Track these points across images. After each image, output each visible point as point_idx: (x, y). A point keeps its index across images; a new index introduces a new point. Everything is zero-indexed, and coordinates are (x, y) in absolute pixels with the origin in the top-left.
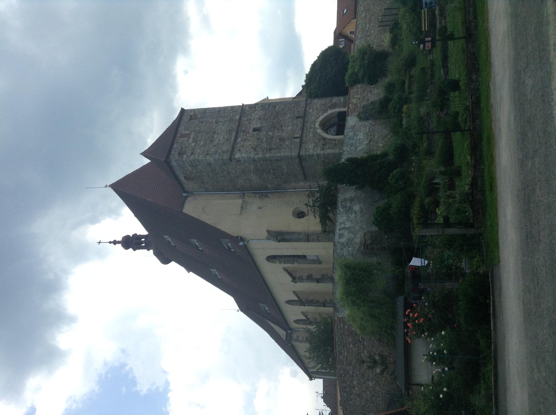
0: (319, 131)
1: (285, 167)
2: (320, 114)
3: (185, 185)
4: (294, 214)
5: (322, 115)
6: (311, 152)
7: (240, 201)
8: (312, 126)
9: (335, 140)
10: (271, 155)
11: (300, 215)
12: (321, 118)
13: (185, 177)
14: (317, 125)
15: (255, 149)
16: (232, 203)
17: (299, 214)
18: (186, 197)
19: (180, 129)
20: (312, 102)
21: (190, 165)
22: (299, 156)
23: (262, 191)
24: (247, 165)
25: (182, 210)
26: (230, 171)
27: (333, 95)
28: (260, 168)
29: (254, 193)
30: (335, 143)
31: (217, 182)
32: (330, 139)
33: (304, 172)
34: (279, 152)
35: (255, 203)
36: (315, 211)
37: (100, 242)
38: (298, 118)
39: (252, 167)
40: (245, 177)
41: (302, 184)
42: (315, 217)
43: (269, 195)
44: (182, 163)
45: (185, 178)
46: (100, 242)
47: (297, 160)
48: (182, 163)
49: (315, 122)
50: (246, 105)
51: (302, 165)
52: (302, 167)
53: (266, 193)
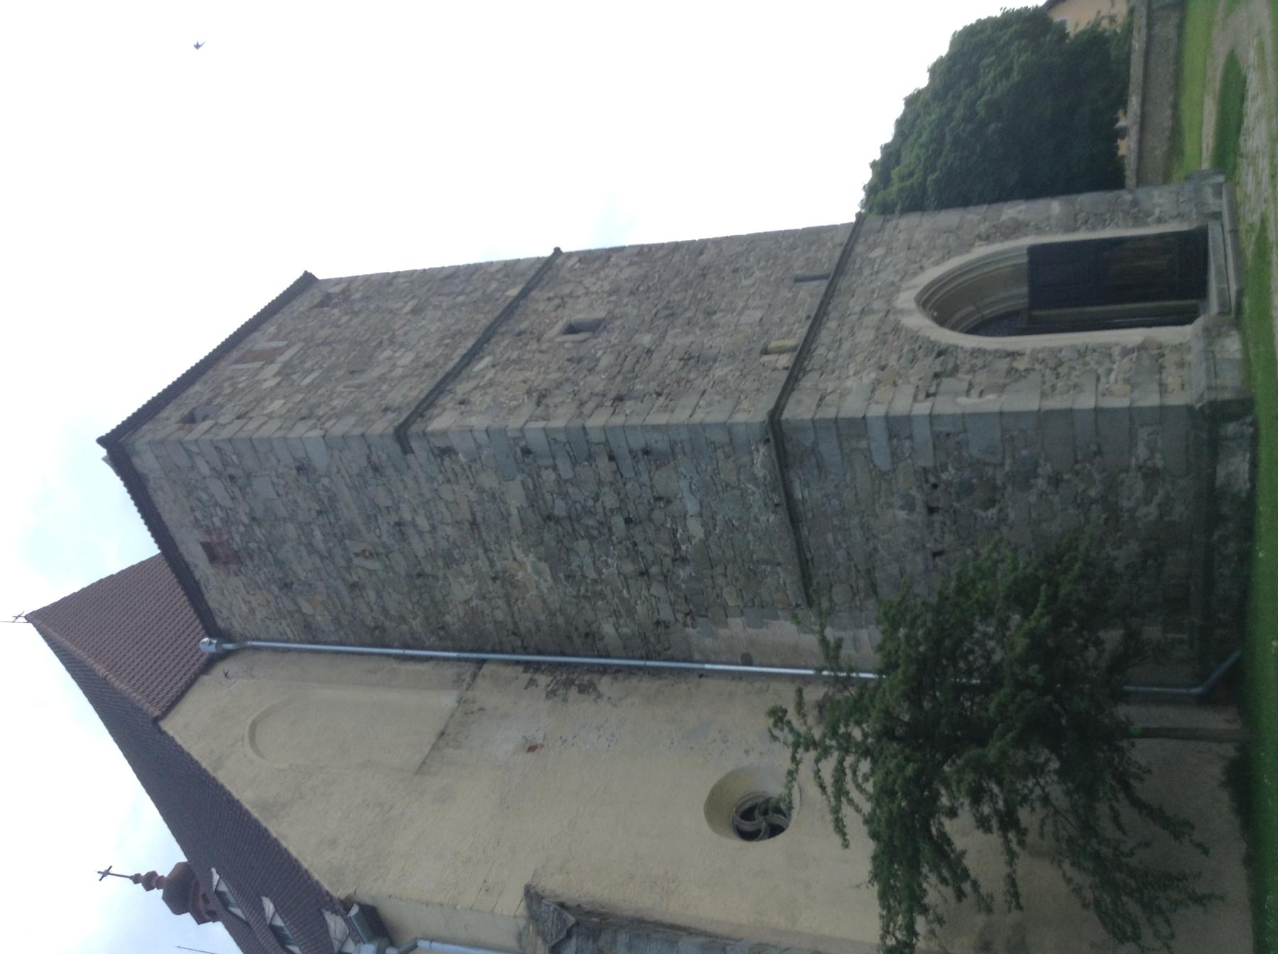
0: (919, 322)
1: (692, 506)
2: (926, 262)
3: (212, 598)
4: (713, 807)
5: (937, 263)
6: (852, 407)
7: (448, 700)
8: (878, 304)
9: (1013, 355)
10: (619, 420)
11: (757, 819)
12: (933, 273)
13: (207, 547)
14: (906, 299)
15: (542, 397)
16: (401, 705)
17: (747, 814)
18: (211, 662)
19: (256, 334)
20: (890, 225)
21: (219, 475)
22: (775, 430)
23: (565, 655)
24: (488, 480)
25: (164, 715)
26: (407, 516)
27: (1004, 194)
28: (560, 509)
29: (527, 665)
30: (1011, 371)
31: (354, 586)
32: (975, 353)
33: (800, 546)
34: (665, 409)
35: (516, 710)
36: (840, 792)
37: (106, 873)
38: (798, 280)
39: (515, 497)
40: (483, 564)
41: (783, 631)
42: (840, 827)
43: (604, 684)
44: (183, 461)
45: (212, 553)
46: (106, 873)
47: (761, 459)
48: (183, 461)
49: (894, 288)
50: (570, 255)
51: (788, 495)
52: (793, 514)
53: (591, 668)
